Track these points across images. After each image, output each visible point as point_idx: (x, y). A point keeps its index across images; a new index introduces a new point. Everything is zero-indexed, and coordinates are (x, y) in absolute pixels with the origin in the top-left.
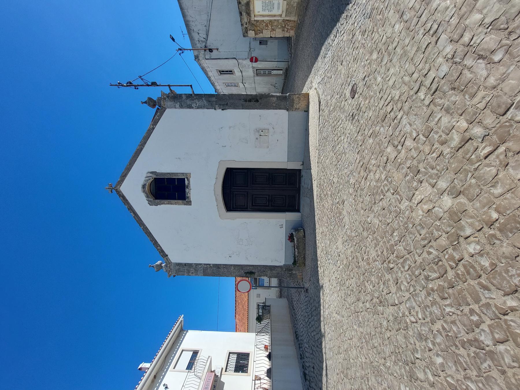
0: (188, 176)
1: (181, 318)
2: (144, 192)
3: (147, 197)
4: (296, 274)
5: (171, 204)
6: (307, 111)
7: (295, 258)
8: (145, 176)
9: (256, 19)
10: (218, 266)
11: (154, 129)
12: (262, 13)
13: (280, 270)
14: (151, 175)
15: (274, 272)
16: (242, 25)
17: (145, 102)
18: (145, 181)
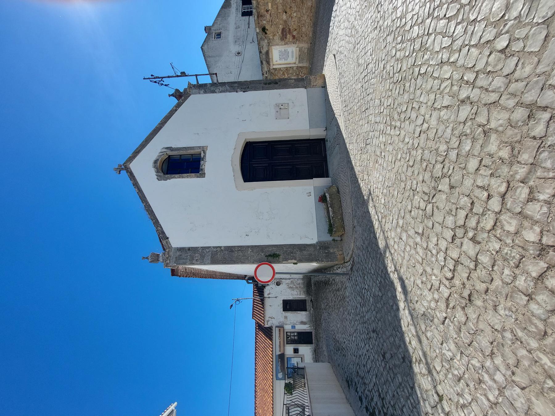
0: (203, 175)
1: (172, 407)
2: (155, 167)
3: (157, 172)
4: (334, 253)
5: (182, 177)
6: (324, 87)
7: (330, 221)
8: (160, 151)
9: (274, 67)
10: (230, 249)
11: (176, 110)
12: (280, 62)
13: (312, 249)
14: (165, 150)
15: (305, 252)
16: (263, 74)
17: (172, 95)
18: (159, 156)
